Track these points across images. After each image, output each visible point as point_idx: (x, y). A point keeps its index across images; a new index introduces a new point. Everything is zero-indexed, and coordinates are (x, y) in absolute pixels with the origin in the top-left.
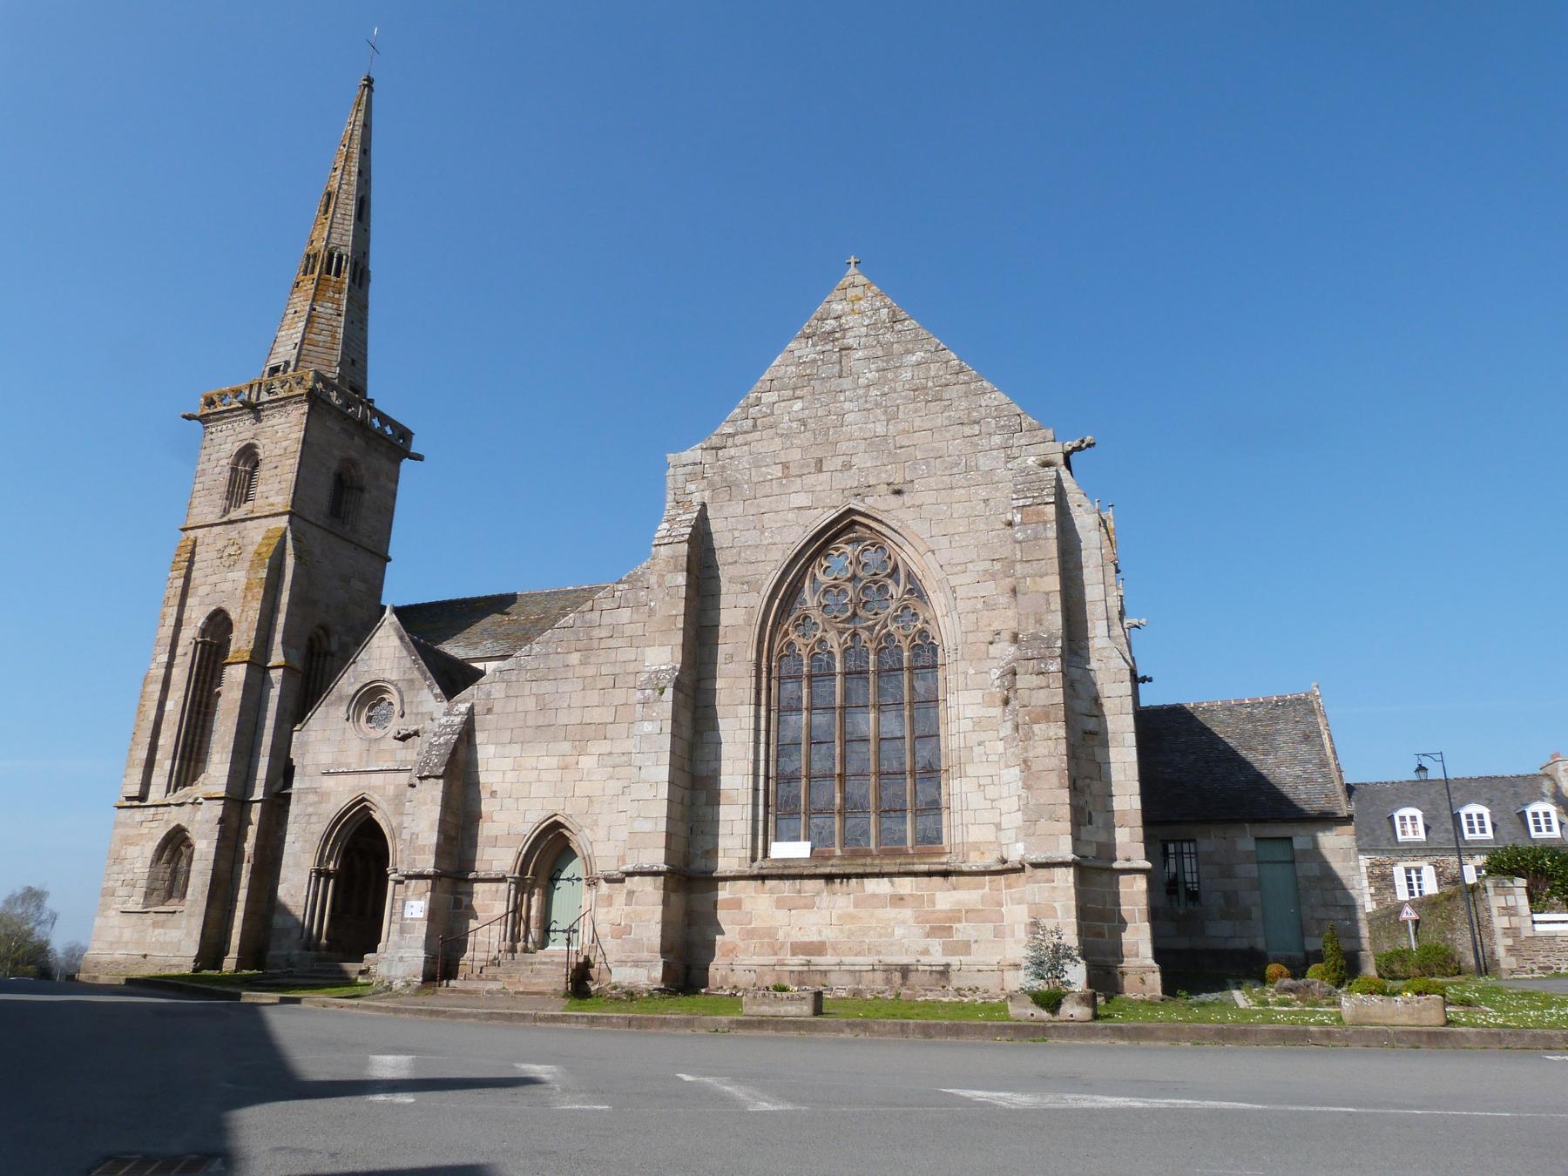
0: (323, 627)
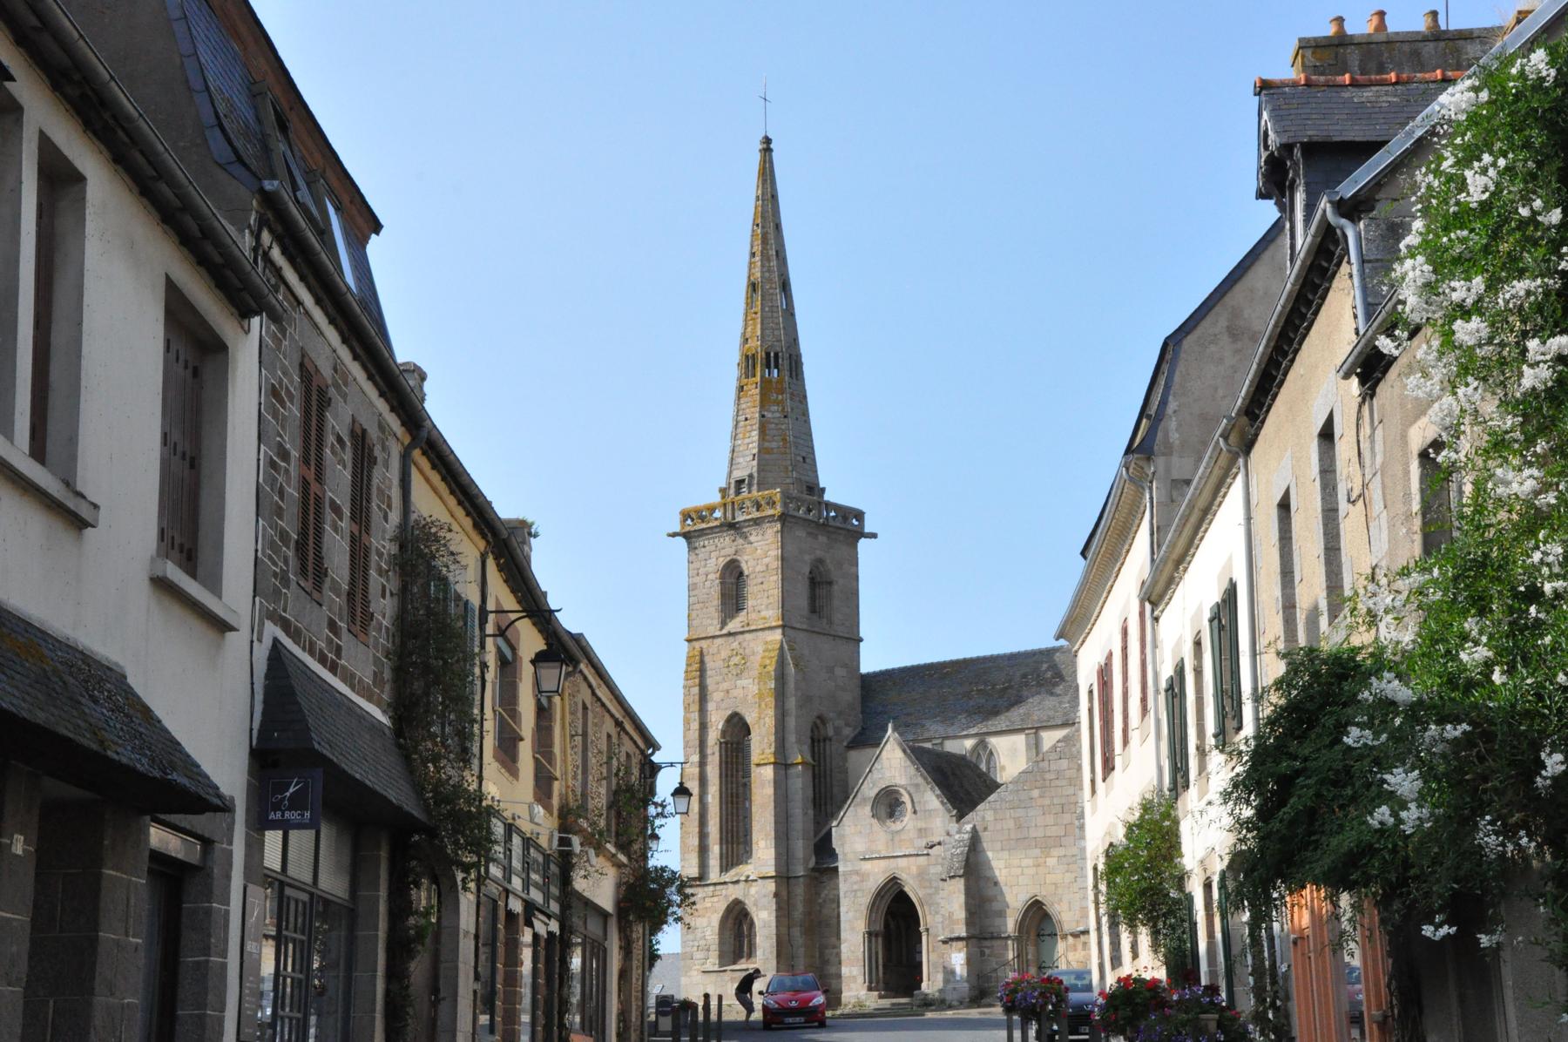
0: (820, 717)
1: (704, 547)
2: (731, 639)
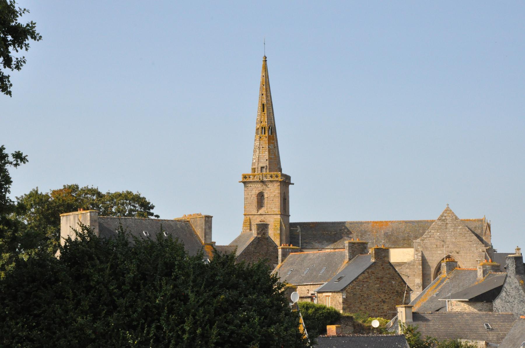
1: (251, 186)
2: (261, 216)
